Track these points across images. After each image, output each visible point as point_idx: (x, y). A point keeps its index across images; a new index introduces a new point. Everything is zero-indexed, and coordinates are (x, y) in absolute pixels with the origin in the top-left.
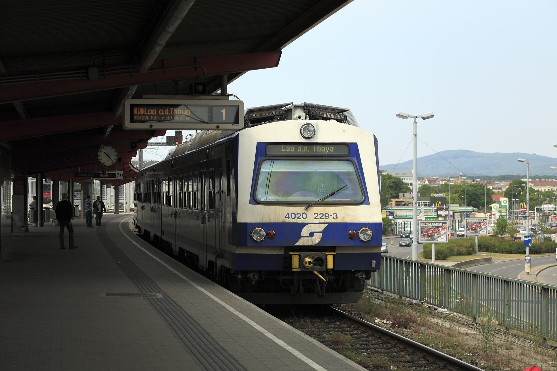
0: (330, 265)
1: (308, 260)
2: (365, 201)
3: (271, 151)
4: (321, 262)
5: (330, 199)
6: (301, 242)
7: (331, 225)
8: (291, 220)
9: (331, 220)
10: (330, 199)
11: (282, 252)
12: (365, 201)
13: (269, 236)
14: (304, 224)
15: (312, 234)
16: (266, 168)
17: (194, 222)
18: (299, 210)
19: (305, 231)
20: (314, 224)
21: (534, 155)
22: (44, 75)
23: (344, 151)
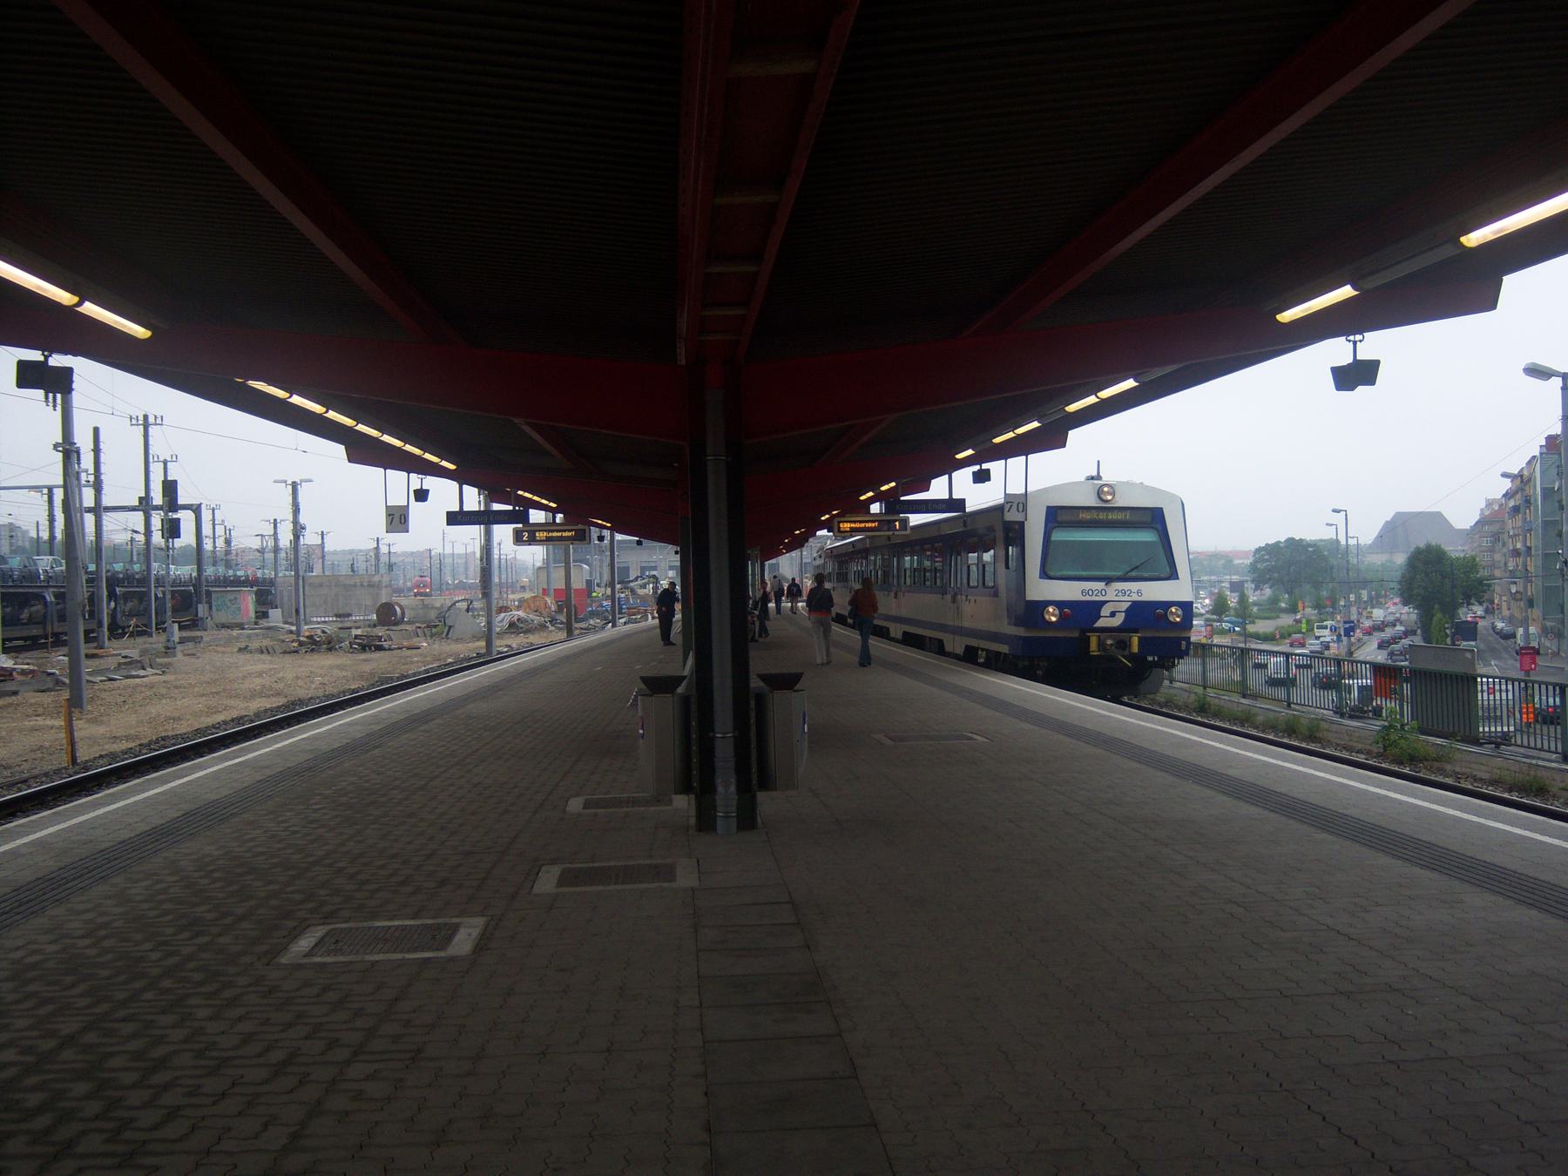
0: (1135, 649)
1: (1109, 642)
2: (1173, 575)
3: (1062, 517)
4: (1123, 645)
5: (1133, 574)
6: (1101, 623)
7: (1135, 603)
8: (1088, 598)
9: (1135, 598)
10: (1133, 574)
11: (1076, 634)
12: (1173, 575)
13: (1062, 617)
14: (1106, 602)
15: (1113, 614)
16: (1058, 536)
17: (555, 647)
18: (1100, 585)
19: (1105, 611)
20: (1118, 597)
21: (1291, 541)
22: (1541, 763)
23: (1147, 518)
